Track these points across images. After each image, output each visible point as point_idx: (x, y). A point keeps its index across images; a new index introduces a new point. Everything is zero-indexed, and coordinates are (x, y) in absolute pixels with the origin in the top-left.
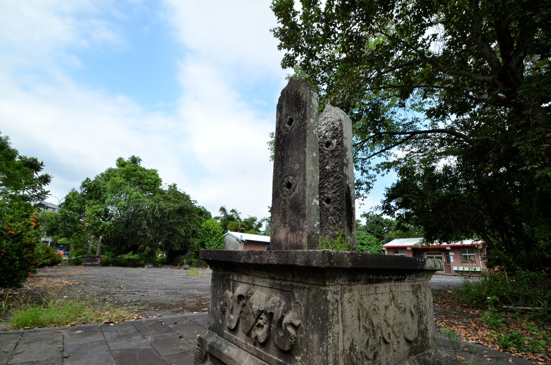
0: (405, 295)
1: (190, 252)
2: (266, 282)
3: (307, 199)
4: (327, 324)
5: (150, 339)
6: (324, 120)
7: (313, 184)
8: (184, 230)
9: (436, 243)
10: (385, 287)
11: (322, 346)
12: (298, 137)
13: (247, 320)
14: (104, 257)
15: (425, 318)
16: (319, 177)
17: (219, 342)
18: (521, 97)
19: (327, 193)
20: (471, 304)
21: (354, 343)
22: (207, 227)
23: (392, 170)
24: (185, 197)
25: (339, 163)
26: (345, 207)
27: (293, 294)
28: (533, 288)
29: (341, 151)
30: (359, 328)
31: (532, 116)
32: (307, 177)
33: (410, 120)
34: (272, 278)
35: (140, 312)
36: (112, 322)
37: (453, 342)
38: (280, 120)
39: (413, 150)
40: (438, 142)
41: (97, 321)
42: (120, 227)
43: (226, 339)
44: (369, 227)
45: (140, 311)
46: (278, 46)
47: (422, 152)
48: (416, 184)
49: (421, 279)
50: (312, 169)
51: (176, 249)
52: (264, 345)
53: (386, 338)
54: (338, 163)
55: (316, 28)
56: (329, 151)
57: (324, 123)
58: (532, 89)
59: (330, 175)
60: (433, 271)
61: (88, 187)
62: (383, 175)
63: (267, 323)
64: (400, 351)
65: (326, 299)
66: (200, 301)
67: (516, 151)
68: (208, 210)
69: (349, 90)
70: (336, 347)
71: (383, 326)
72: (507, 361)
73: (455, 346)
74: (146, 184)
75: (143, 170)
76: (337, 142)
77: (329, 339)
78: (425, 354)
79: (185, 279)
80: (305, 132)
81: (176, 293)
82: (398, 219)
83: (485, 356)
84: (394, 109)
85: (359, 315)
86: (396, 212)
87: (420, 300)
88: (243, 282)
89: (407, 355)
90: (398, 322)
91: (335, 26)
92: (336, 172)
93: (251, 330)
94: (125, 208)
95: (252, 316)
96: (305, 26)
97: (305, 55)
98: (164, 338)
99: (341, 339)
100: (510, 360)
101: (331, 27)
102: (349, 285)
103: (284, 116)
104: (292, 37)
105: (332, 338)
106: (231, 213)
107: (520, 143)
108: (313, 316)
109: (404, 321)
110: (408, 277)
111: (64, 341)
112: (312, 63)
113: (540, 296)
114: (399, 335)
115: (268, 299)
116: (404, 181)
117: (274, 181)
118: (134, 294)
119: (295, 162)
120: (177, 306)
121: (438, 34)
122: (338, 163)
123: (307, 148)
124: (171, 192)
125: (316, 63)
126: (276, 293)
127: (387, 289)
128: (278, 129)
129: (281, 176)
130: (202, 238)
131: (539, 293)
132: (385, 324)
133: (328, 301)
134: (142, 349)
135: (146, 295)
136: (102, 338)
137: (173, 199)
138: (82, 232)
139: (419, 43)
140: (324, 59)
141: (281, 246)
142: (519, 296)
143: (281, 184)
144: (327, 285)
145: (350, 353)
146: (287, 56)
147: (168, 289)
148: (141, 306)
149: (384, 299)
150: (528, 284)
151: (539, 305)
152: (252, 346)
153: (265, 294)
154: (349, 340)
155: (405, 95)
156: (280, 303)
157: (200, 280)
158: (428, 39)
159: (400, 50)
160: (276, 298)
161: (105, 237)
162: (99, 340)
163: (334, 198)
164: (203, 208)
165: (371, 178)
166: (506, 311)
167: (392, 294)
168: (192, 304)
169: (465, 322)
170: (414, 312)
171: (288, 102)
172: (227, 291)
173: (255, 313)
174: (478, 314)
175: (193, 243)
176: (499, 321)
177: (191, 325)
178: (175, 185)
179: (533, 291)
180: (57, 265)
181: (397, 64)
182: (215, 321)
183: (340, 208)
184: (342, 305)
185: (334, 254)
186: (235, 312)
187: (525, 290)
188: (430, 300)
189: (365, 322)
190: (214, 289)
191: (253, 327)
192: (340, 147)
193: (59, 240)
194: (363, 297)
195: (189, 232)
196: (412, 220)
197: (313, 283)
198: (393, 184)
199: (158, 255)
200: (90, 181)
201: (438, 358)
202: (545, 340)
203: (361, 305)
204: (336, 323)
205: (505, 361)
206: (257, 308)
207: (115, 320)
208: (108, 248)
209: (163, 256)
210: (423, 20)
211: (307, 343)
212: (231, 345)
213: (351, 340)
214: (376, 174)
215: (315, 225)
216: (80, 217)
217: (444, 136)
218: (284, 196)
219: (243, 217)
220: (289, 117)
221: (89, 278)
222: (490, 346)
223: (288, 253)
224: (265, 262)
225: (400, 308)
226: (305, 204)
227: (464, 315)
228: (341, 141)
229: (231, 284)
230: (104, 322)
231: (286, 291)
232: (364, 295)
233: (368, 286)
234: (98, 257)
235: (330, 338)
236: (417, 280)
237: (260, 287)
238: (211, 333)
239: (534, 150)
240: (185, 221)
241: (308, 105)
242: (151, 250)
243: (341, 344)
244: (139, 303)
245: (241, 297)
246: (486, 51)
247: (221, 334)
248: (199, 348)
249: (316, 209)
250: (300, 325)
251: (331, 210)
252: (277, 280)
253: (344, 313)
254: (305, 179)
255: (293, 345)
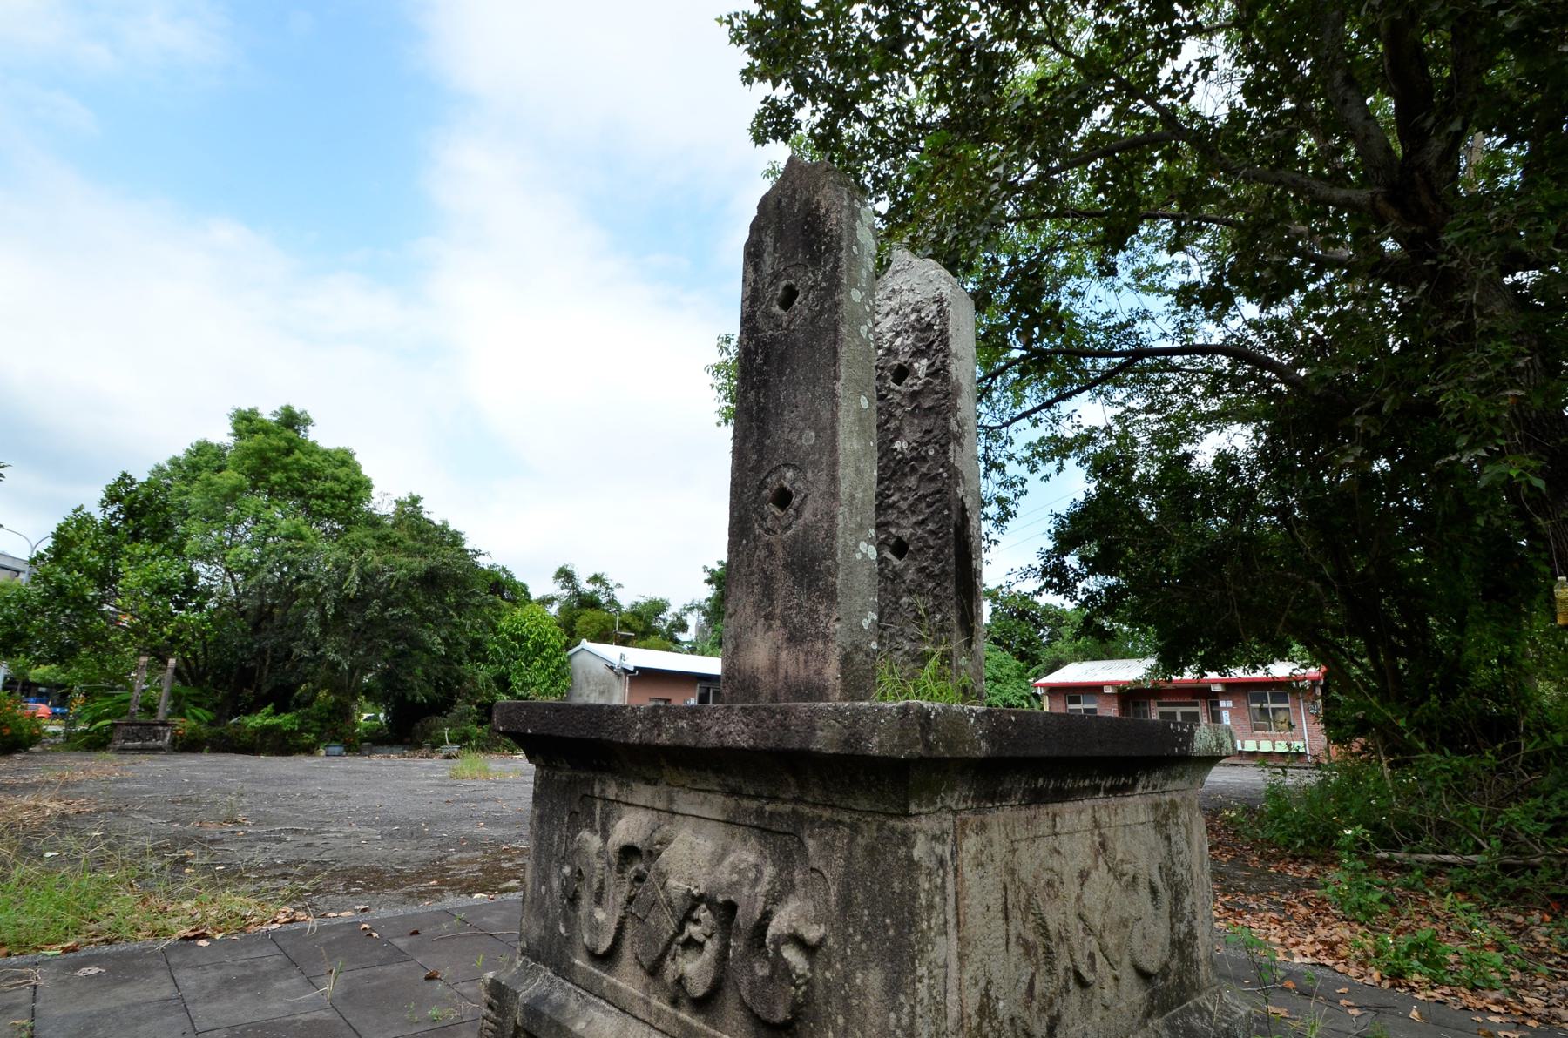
0: (1134, 834)
1: (461, 707)
2: (712, 805)
3: (841, 540)
4: (913, 938)
5: (329, 987)
6: (889, 298)
7: (859, 495)
8: (444, 639)
9: (1189, 675)
10: (1080, 812)
11: (897, 1008)
12: (812, 347)
13: (649, 926)
14: (184, 725)
15: (1187, 903)
16: (875, 473)
17: (556, 996)
18: (1452, 254)
19: (898, 525)
20: (1288, 848)
21: (992, 993)
22: (517, 629)
23: (1070, 463)
24: (448, 539)
25: (935, 432)
26: (951, 568)
27: (801, 842)
28: (1462, 801)
29: (941, 396)
30: (1007, 943)
31: (1480, 310)
32: (840, 472)
33: (1122, 318)
34: (733, 792)
35: (299, 899)
36: (203, 936)
37: (1259, 967)
38: (755, 291)
39: (1132, 404)
40: (1201, 383)
41: (155, 934)
42: (234, 630)
43: (579, 986)
44: (998, 628)
45: (298, 895)
46: (744, 72)
47: (1159, 412)
48: (1137, 503)
49: (1179, 784)
50: (856, 446)
51: (418, 699)
52: (704, 1004)
53: (1083, 970)
54: (931, 431)
55: (859, 21)
56: (904, 396)
57: (888, 308)
58: (1485, 228)
59: (907, 469)
60: (1211, 760)
61: (127, 500)
62: (1047, 478)
63: (716, 936)
64: (1122, 1004)
65: (910, 859)
66: (495, 859)
67: (1429, 408)
68: (518, 578)
69: (958, 215)
70: (938, 1010)
71: (1074, 932)
72: (1406, 1016)
73: (1262, 977)
74: (321, 497)
75: (313, 449)
76: (928, 367)
77: (918, 985)
78: (1189, 1011)
79: (447, 790)
80: (836, 331)
81: (417, 836)
82: (1086, 606)
83: (1343, 1002)
84: (1077, 281)
85: (1006, 903)
86: (1080, 586)
87: (1174, 850)
88: (637, 806)
89: (1139, 1017)
90: (1117, 919)
91: (918, 18)
92: (924, 459)
93: (662, 957)
94: (249, 570)
95: (668, 912)
96: (826, 15)
97: (823, 106)
98: (376, 983)
99: (952, 984)
100: (1414, 1014)
101: (905, 22)
102: (977, 811)
103: (768, 280)
104: (785, 44)
105: (926, 981)
106: (590, 588)
107: (1444, 386)
108: (866, 912)
109: (1134, 913)
110: (1142, 781)
111: (38, 1005)
112: (846, 132)
113: (1479, 823)
114: (1118, 958)
115: (719, 858)
116: (1104, 494)
117: (734, 485)
118: (279, 841)
119: (801, 425)
120: (420, 876)
121: (1216, 57)
122: (931, 431)
123: (842, 381)
124: (401, 522)
125: (859, 128)
126: (745, 841)
127: (1086, 818)
128: (748, 321)
129: (756, 469)
130: (500, 662)
131: (1477, 814)
132: (1081, 926)
133: (916, 864)
134: (304, 1023)
135: (318, 842)
136: (167, 991)
137: (410, 542)
138: (108, 644)
139: (1162, 84)
140: (881, 118)
141: (755, 688)
142: (1423, 822)
143: (759, 493)
144: (911, 815)
145: (980, 1025)
146: (771, 103)
147: (392, 822)
148: (304, 878)
149: (1078, 850)
150: (1448, 790)
151: (1478, 849)
152: (665, 1007)
153: (709, 844)
154: (977, 984)
155: (1115, 237)
156: (760, 872)
157: (494, 792)
158: (1187, 71)
159: (1107, 104)
160: (746, 854)
161: (185, 660)
162: (158, 996)
163: (919, 539)
164: (504, 569)
165: (1013, 485)
166: (1384, 865)
167: (1101, 835)
168: (470, 867)
169: (1277, 903)
170: (1160, 885)
171: (780, 236)
172: (585, 834)
173: (677, 903)
174: (1311, 878)
175: (473, 681)
176: (1375, 898)
177: (465, 936)
178: (415, 501)
179: (1459, 809)
180: (26, 749)
181: (1096, 143)
182: (545, 927)
183: (936, 569)
184: (956, 876)
185: (938, 714)
186: (611, 901)
187: (1440, 807)
188: (1201, 846)
189: (1024, 922)
190: (541, 828)
191: (668, 947)
192: (937, 381)
193: (34, 671)
194: (1016, 845)
195: (458, 644)
196: (1123, 607)
197: (868, 807)
198: (1074, 503)
199: (360, 716)
200: (133, 483)
201: (1226, 1021)
202: (1499, 951)
203: (1012, 872)
204: (939, 934)
205: (1401, 1016)
206: (684, 886)
207: (214, 929)
208: (195, 695)
209: (376, 718)
210: (1177, 15)
211: (846, 998)
212: (598, 1006)
213: (982, 984)
214: (1027, 475)
215: (866, 624)
216: (103, 597)
217: (1223, 363)
218: (768, 531)
219: (627, 598)
220: (784, 283)
221: (134, 792)
222: (1353, 972)
223: (785, 713)
224: (710, 740)
225: (1122, 875)
226: (833, 556)
227: (1272, 880)
228: (943, 363)
229: (598, 812)
230: (176, 937)
231: (779, 833)
232: (1021, 840)
233: (1032, 811)
234: (164, 724)
235: (920, 982)
236: (1167, 788)
237: (692, 821)
238: (531, 968)
239: (1482, 407)
240: (446, 612)
241: (844, 244)
242: (338, 701)
243: (952, 997)
244: (297, 871)
245: (629, 853)
246: (1355, 115)
247: (563, 970)
248: (493, 1015)
249: (867, 572)
250: (822, 940)
251: (910, 575)
252: (749, 797)
253: (964, 899)
254: (834, 479)
255: (801, 1005)
